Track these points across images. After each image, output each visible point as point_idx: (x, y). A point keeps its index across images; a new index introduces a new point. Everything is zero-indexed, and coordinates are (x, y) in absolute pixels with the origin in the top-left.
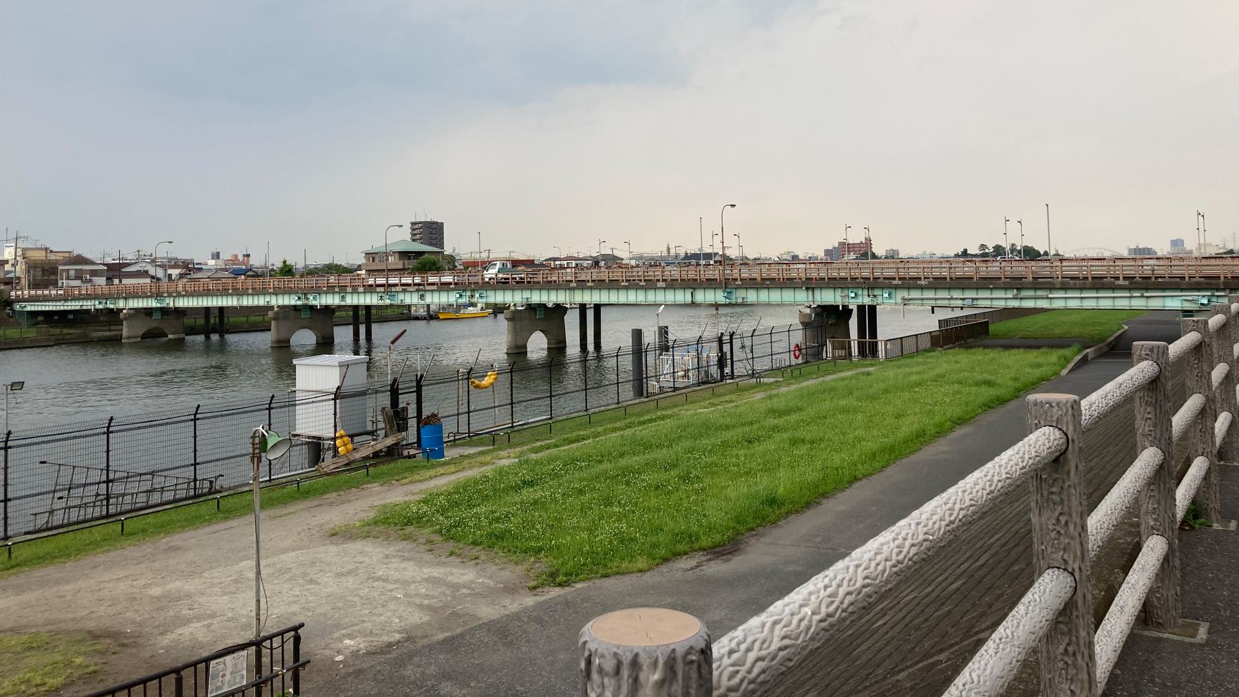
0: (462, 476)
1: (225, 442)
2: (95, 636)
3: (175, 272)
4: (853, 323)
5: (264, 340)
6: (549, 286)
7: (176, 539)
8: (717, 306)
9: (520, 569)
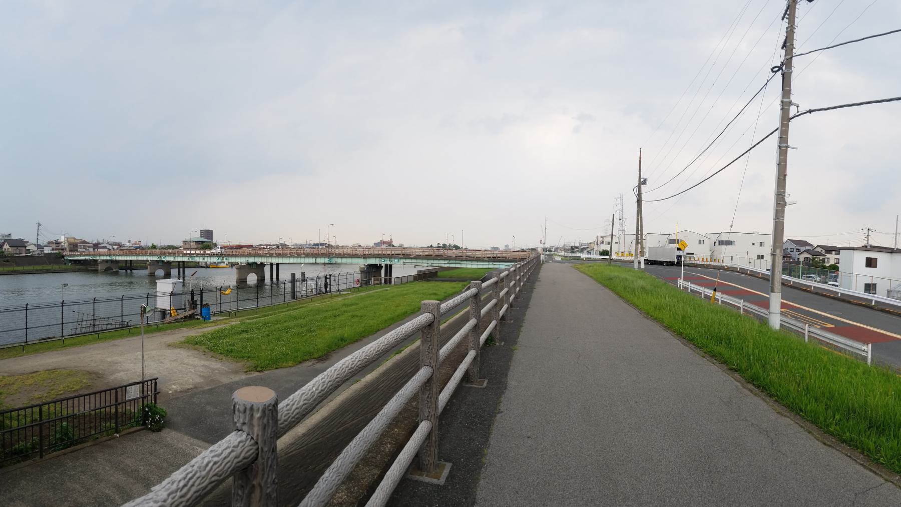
0: (217, 328)
1: (132, 309)
2: (90, 373)
3: (115, 247)
4: (383, 271)
5: (146, 272)
6: (259, 256)
7: (116, 342)
8: (325, 264)
9: (239, 364)
